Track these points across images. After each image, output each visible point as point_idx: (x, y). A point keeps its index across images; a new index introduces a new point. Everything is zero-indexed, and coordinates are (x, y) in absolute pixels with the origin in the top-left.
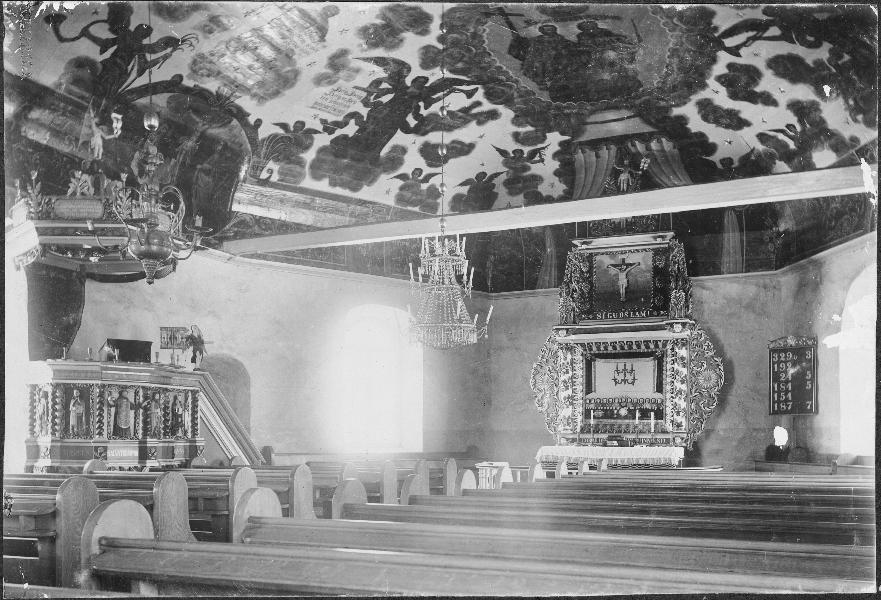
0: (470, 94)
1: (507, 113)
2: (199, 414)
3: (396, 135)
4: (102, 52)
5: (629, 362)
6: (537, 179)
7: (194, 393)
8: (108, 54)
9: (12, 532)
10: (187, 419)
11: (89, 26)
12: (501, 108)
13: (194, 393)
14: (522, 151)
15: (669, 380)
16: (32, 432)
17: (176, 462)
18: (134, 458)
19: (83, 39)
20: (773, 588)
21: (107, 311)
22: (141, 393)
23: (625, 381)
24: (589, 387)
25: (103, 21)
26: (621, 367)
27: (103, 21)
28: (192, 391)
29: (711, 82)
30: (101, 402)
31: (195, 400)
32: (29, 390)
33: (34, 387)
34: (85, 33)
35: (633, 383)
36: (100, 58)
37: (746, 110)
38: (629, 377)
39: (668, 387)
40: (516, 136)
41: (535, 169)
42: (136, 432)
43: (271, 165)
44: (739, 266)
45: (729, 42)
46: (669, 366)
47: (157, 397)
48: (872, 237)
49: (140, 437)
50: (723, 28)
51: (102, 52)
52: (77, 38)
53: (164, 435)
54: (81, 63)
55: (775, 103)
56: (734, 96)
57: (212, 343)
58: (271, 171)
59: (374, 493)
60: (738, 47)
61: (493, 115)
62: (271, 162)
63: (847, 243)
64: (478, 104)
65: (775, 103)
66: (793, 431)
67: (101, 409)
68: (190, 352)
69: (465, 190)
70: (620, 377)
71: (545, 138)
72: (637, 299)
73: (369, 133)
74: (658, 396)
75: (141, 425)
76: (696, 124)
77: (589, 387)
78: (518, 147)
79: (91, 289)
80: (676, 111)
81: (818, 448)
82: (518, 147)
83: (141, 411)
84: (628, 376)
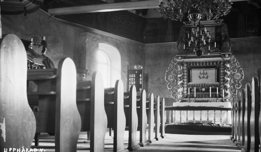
23: (204, 77)
24: (189, 80)
35: (207, 78)
70: (202, 76)
74: (217, 83)
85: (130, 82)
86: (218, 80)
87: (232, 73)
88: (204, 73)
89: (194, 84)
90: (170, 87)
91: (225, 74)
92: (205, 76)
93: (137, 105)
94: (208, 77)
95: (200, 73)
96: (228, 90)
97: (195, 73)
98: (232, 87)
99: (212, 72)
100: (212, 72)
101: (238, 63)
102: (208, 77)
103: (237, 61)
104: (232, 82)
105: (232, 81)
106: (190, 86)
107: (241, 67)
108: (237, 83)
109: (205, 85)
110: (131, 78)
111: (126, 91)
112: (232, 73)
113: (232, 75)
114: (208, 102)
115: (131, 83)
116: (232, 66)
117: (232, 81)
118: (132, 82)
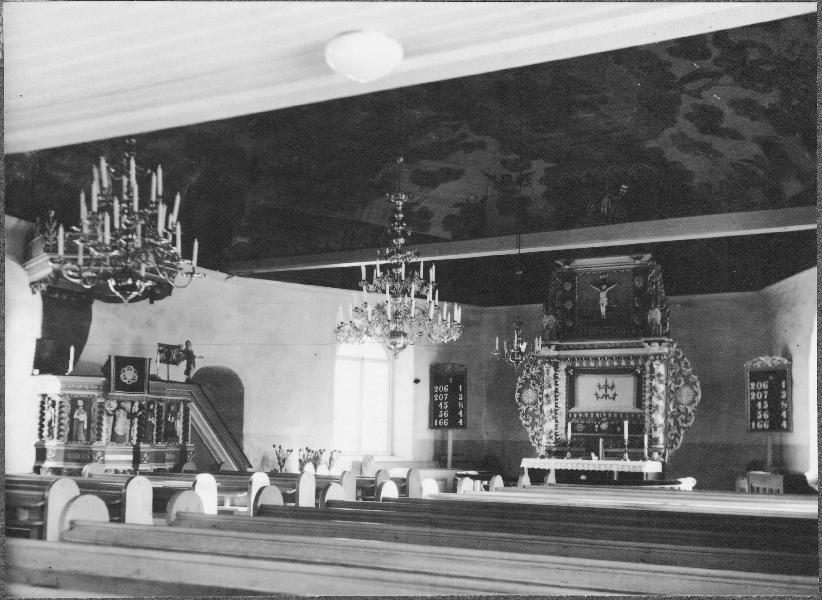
0: (455, 128)
1: (492, 143)
2: (190, 422)
3: (95, 328)
5: (611, 379)
6: (525, 201)
7: (185, 402)
10: (179, 426)
12: (488, 139)
13: (185, 402)
14: (510, 176)
15: (647, 395)
16: (41, 436)
17: (168, 466)
18: (128, 461)
20: (795, 583)
21: (111, 330)
22: (137, 404)
23: (606, 396)
24: (571, 401)
26: (602, 383)
28: (184, 401)
29: (680, 119)
30: (101, 412)
31: (187, 410)
32: (40, 399)
33: (44, 396)
35: (614, 398)
37: (718, 143)
38: (610, 393)
39: (647, 403)
40: (504, 163)
41: (526, 192)
42: (131, 439)
45: (688, 87)
46: (648, 382)
47: (151, 407)
49: (135, 442)
50: (680, 75)
53: (157, 441)
55: (742, 138)
56: (703, 131)
57: (201, 357)
59: (368, 489)
60: (700, 90)
61: (482, 146)
64: (464, 136)
65: (742, 138)
66: (583, 481)
67: (100, 419)
68: (183, 365)
69: (456, 211)
70: (602, 392)
71: (530, 166)
72: (189, 460)
74: (638, 410)
75: (136, 432)
76: (673, 154)
77: (571, 401)
78: (506, 172)
79: (98, 309)
80: (651, 144)
82: (506, 172)
83: (136, 420)
84: (609, 391)
85: (766, 397)
86: (639, 403)
87: (672, 388)
88: (606, 386)
89: (585, 410)
90: (527, 420)
91: (653, 389)
92: (610, 393)
93: (621, 474)
94: (615, 395)
95: (599, 386)
96: (658, 429)
97: (587, 385)
98: (671, 421)
99: (625, 385)
100: (625, 385)
101: (686, 363)
102: (615, 395)
103: (684, 357)
104: (672, 410)
105: (671, 406)
106: (573, 417)
107: (694, 372)
108: (683, 414)
109: (607, 416)
110: (439, 393)
111: (787, 434)
112: (672, 388)
113: (671, 391)
114: (638, 460)
115: (764, 395)
116: (671, 369)
117: (671, 406)
118: (753, 394)
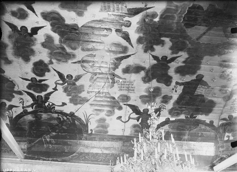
4: (138, 121)
8: (140, 121)
9: (236, 34)
11: (129, 116)
19: (130, 120)
25: (132, 113)
27: (132, 113)
34: (129, 118)
36: (138, 123)
43: (227, 134)
44: (218, 65)
48: (236, 154)
51: (138, 121)
52: (129, 120)
54: (135, 126)
58: (229, 137)
62: (226, 133)
63: (32, 160)
73: (58, 132)
81: (180, 75)
